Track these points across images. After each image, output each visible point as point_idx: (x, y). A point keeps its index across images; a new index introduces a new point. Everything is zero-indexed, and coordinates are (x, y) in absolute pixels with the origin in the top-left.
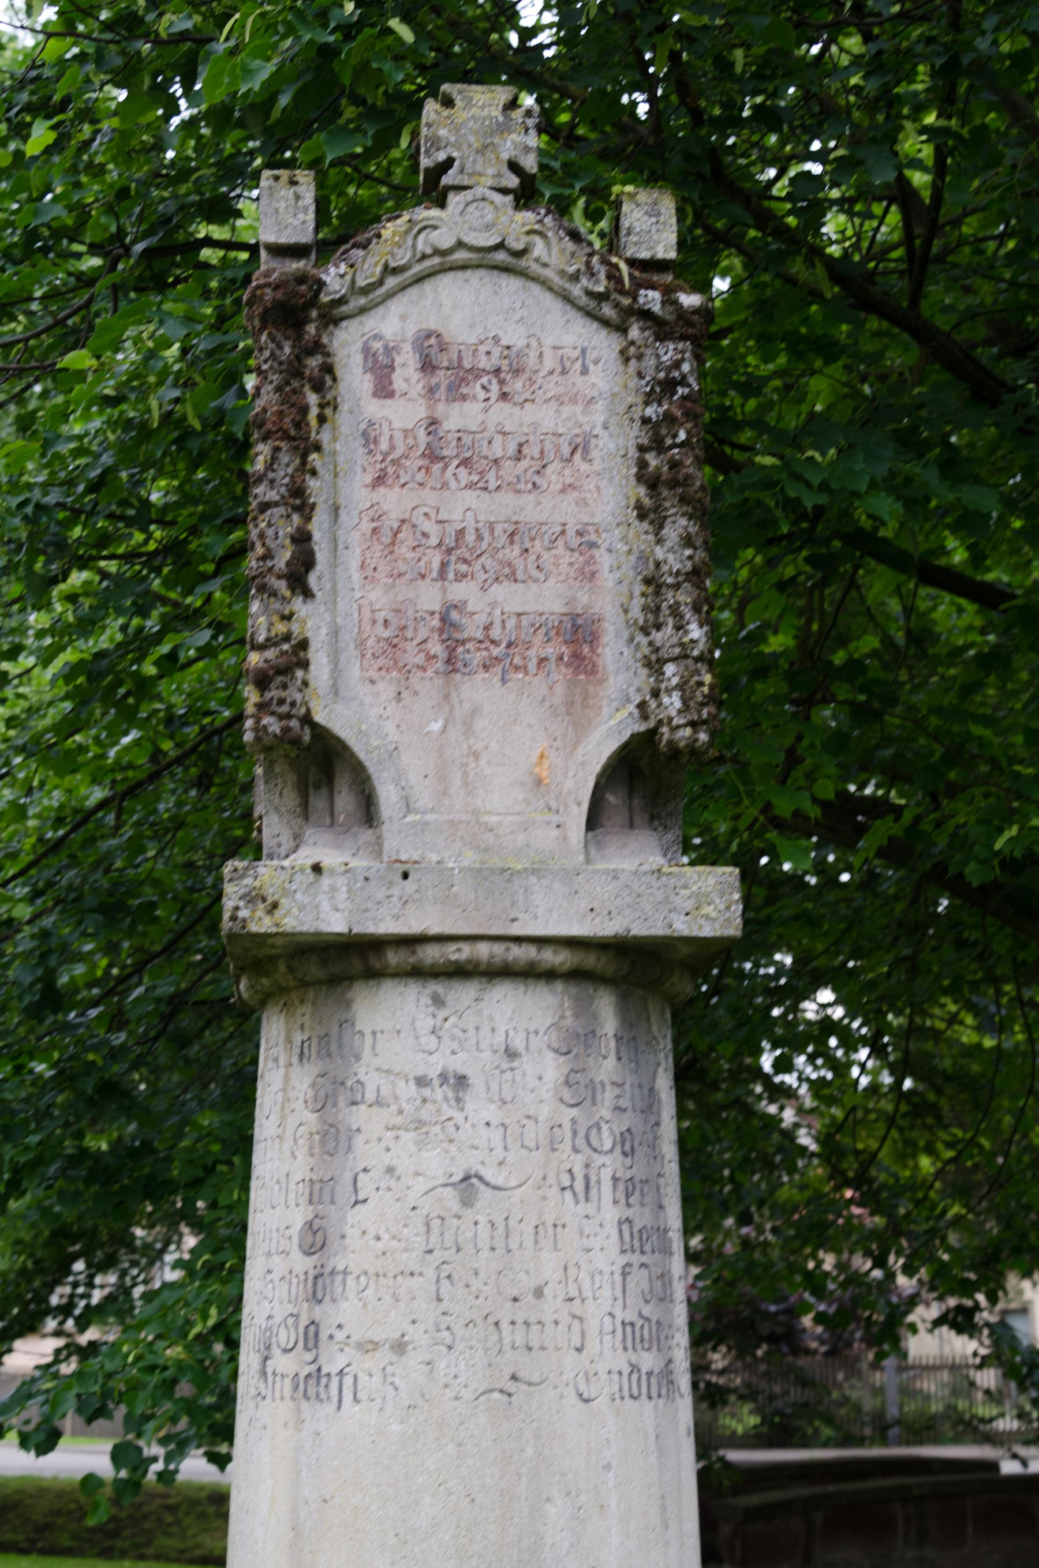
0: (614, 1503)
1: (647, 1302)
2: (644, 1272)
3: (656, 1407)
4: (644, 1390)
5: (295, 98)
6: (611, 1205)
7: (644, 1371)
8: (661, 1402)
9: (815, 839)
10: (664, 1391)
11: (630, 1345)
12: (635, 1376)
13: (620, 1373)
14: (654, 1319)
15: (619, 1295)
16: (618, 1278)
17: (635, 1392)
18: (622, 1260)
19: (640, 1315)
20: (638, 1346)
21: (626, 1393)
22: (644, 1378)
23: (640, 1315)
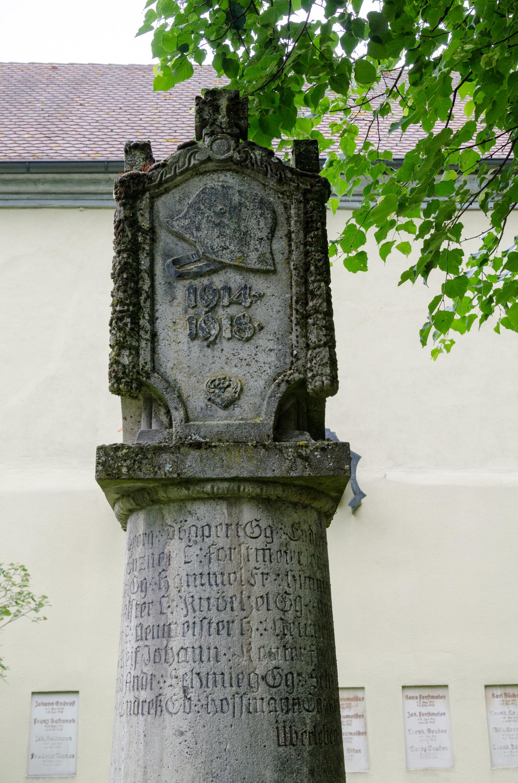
0: (123, 768)
1: (146, 665)
2: (146, 649)
3: (146, 720)
4: (140, 711)
5: (487, 114)
6: (134, 618)
7: (141, 701)
8: (150, 716)
9: (314, 57)
10: (152, 711)
11: (136, 687)
12: (136, 703)
13: (131, 702)
14: (150, 673)
15: (133, 663)
16: (134, 654)
17: (136, 712)
18: (135, 646)
19: (142, 672)
20: (140, 689)
21: (132, 712)
22: (141, 704)
23: (142, 672)
